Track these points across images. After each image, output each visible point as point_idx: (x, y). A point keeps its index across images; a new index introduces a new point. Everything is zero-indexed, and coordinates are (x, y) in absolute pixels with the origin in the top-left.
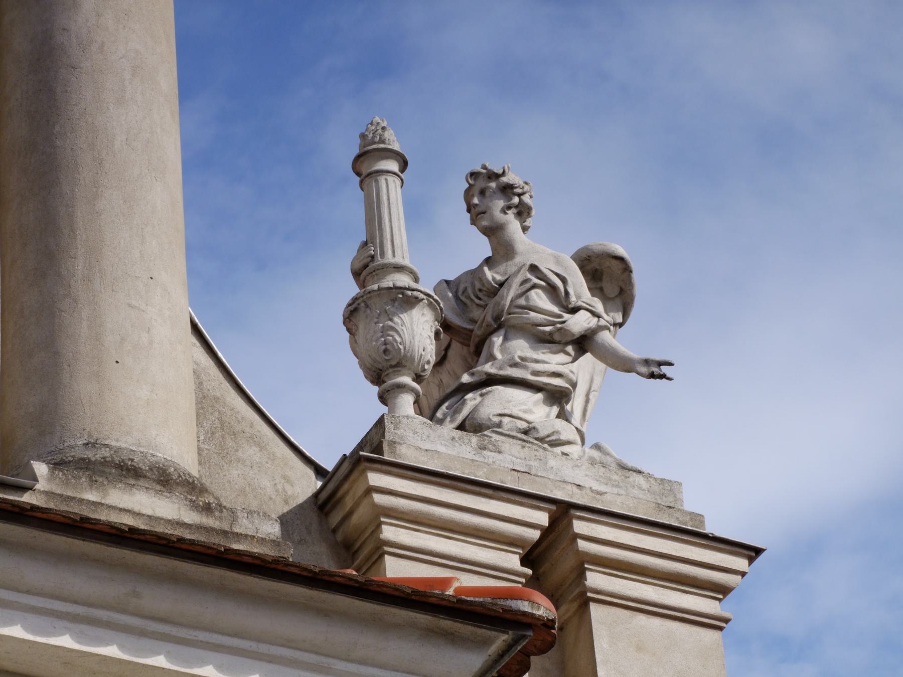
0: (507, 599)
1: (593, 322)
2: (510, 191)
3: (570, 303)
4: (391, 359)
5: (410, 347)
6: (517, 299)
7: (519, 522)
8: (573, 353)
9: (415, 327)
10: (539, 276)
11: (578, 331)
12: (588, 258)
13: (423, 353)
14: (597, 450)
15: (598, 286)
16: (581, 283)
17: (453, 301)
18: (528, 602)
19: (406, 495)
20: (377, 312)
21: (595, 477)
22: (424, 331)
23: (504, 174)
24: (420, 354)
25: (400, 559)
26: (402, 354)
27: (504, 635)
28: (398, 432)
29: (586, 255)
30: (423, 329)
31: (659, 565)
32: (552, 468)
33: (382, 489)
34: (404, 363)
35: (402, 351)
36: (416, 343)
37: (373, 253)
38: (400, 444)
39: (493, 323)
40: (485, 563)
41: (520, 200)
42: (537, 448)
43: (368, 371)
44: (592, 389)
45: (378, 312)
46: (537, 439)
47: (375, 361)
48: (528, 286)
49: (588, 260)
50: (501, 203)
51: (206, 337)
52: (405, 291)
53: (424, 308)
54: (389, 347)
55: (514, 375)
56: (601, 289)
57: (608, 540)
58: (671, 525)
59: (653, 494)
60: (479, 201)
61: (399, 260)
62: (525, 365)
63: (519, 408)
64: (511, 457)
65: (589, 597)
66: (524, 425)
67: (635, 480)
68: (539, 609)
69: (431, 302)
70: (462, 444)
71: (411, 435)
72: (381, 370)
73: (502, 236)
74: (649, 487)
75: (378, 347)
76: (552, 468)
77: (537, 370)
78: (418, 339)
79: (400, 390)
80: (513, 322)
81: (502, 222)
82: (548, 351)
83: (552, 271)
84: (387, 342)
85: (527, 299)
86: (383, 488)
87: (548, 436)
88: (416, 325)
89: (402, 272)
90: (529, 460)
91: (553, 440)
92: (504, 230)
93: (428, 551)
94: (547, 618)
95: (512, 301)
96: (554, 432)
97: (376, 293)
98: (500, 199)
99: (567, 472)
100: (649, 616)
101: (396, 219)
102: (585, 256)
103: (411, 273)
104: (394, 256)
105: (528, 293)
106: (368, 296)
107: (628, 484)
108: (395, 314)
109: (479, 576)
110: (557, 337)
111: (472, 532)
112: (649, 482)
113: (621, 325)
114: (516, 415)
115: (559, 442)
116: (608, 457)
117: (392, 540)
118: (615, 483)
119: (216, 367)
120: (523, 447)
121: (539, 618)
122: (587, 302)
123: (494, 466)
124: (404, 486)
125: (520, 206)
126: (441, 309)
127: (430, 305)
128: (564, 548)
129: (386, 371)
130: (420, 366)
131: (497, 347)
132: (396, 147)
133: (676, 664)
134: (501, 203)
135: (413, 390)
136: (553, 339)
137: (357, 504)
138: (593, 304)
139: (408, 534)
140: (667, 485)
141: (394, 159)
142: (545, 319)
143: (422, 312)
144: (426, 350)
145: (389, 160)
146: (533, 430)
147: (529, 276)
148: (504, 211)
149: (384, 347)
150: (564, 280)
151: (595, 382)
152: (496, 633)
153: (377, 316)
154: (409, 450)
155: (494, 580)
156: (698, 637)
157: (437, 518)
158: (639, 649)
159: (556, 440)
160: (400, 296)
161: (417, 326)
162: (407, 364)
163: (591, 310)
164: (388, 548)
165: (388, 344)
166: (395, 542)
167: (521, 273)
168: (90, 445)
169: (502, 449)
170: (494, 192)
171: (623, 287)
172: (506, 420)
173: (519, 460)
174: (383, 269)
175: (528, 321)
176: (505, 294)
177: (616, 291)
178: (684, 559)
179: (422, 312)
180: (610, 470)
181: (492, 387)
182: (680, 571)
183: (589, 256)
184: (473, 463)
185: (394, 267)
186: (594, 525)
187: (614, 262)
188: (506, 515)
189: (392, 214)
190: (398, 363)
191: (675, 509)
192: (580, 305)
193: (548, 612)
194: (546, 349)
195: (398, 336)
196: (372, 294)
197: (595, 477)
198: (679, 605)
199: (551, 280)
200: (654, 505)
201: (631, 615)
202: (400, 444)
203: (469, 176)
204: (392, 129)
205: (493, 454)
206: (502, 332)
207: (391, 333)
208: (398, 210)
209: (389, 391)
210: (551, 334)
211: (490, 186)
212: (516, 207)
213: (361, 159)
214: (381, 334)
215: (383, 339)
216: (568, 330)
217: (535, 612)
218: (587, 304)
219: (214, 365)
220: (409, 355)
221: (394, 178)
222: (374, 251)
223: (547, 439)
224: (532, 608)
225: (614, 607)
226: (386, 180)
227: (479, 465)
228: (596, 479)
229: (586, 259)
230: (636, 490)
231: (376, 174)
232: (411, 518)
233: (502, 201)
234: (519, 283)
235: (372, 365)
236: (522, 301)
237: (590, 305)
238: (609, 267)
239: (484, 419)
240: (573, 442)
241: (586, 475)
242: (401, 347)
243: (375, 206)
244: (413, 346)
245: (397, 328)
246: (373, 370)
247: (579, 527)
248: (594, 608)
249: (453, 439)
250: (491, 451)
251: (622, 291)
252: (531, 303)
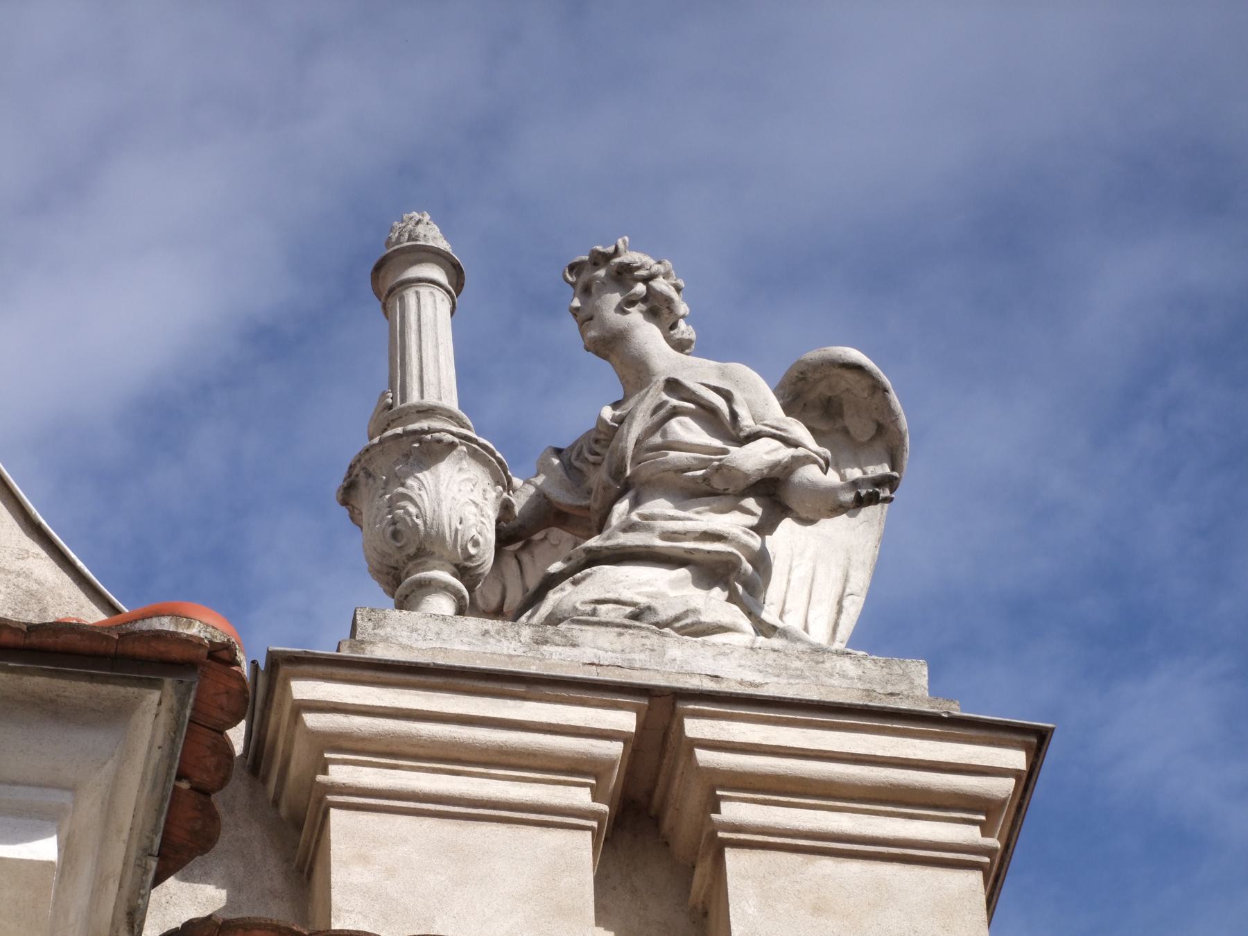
0: (136, 621)
1: (785, 453)
2: (628, 276)
3: (741, 430)
4: (406, 545)
5: (433, 519)
6: (648, 438)
7: (582, 732)
8: (759, 510)
9: (442, 489)
10: (685, 396)
11: (754, 468)
12: (801, 376)
13: (459, 527)
14: (782, 637)
15: (838, 426)
16: (766, 400)
17: (561, 472)
18: (169, 618)
19: (364, 709)
20: (382, 479)
21: (758, 667)
22: (461, 493)
23: (616, 252)
24: (453, 528)
25: (358, 812)
26: (422, 533)
27: (152, 691)
28: (381, 632)
29: (798, 372)
30: (460, 490)
31: (854, 775)
32: (675, 660)
33: (319, 704)
34: (428, 547)
35: (422, 527)
36: (445, 513)
37: (390, 401)
38: (371, 643)
39: (612, 482)
40: (516, 801)
41: (649, 288)
42: (649, 634)
43: (380, 576)
44: (848, 591)
45: (384, 478)
46: (657, 624)
47: (384, 555)
48: (662, 412)
49: (803, 379)
50: (616, 298)
51: (58, 542)
52: (424, 436)
53: (461, 459)
54: (399, 526)
55: (629, 543)
56: (846, 431)
57: (751, 744)
58: (867, 706)
59: (868, 682)
60: (581, 302)
61: (431, 399)
62: (648, 525)
63: (638, 591)
64: (595, 650)
65: (721, 838)
66: (629, 610)
67: (835, 666)
68: (190, 625)
69: (476, 450)
70: (503, 640)
71: (405, 634)
72: (395, 568)
73: (626, 351)
74: (861, 673)
75: (384, 530)
76: (675, 660)
77: (671, 530)
78: (449, 506)
79: (424, 590)
80: (645, 475)
81: (620, 327)
82: (708, 508)
83: (708, 386)
84: (396, 519)
85: (664, 435)
86: (320, 701)
87: (677, 619)
88: (445, 485)
89: (434, 417)
90: (629, 653)
91: (687, 624)
92: (627, 340)
93: (408, 792)
94: (211, 642)
95: (638, 442)
96: (687, 611)
97: (378, 449)
98: (614, 292)
99: (702, 664)
100: (840, 859)
101: (429, 346)
102: (797, 374)
103: (451, 417)
104: (422, 397)
105: (666, 425)
106: (367, 456)
107: (821, 672)
108: (408, 475)
109: (509, 825)
110: (717, 484)
111: (496, 759)
112: (862, 666)
113: (890, 482)
114: (629, 600)
115: (701, 627)
116: (798, 644)
117: (339, 781)
118: (794, 673)
119: (74, 585)
120: (621, 634)
121: (189, 641)
122: (772, 424)
123: (553, 661)
124: (359, 696)
125: (651, 298)
126: (500, 462)
127: (474, 454)
128: (683, 773)
129: (404, 568)
130: (459, 550)
131: (617, 516)
132: (443, 245)
133: (890, 928)
134: (616, 298)
135: (445, 588)
136: (712, 487)
137: (290, 742)
138: (784, 426)
139: (377, 774)
140: (896, 667)
141: (445, 270)
142: (695, 458)
143: (458, 467)
144: (464, 522)
145: (424, 264)
146: (648, 612)
147: (665, 397)
148: (621, 309)
149: (391, 528)
150: (728, 396)
151: (852, 579)
152: (136, 690)
153: (383, 485)
154: (388, 650)
155: (539, 828)
156: (936, 884)
157: (425, 740)
158: (817, 910)
159: (693, 624)
160: (416, 445)
161: (447, 486)
162: (436, 549)
163: (780, 436)
164: (336, 797)
165: (398, 522)
166: (344, 784)
167: (649, 395)
168: (144, 878)
169: (580, 640)
170: (603, 283)
171: (880, 419)
172: (600, 607)
173: (610, 653)
174: (400, 417)
175: (667, 466)
176: (625, 432)
177: (871, 430)
178: (900, 761)
179: (458, 467)
180: (786, 655)
181: (593, 568)
182: (895, 782)
183: (802, 373)
184: (511, 660)
185: (418, 412)
186: (724, 724)
187: (850, 376)
188: (554, 721)
189: (422, 339)
190: (418, 549)
191: (901, 696)
192: (759, 430)
193: (210, 629)
194: (701, 506)
195: (413, 506)
196: (372, 452)
197: (758, 667)
198: (893, 834)
199: (703, 398)
200: (860, 693)
201: (806, 861)
202: (371, 643)
203: (567, 270)
204: (435, 219)
205: (560, 649)
206: (631, 494)
207: (402, 503)
208: (436, 333)
209: (407, 596)
210: (705, 478)
211: (594, 276)
212: (644, 300)
213: (382, 274)
214: (389, 509)
215: (390, 516)
216: (733, 467)
217: (180, 630)
218: (773, 427)
219: (71, 581)
220: (433, 532)
221: (432, 290)
222: (392, 398)
223: (678, 625)
224: (177, 625)
225: (773, 852)
226: (417, 293)
227: (522, 662)
228: (758, 669)
229: (800, 380)
230: (835, 680)
231: (400, 289)
232: (381, 748)
233: (618, 294)
234: (649, 412)
235: (380, 563)
236: (657, 439)
237: (777, 429)
238: (847, 390)
239: (565, 610)
240: (732, 627)
241: (740, 666)
242: (419, 521)
243: (398, 334)
244: (439, 516)
245: (410, 493)
246: (385, 571)
247: (694, 728)
248: (730, 855)
249: (486, 633)
250: (559, 645)
251: (881, 429)
252: (671, 438)
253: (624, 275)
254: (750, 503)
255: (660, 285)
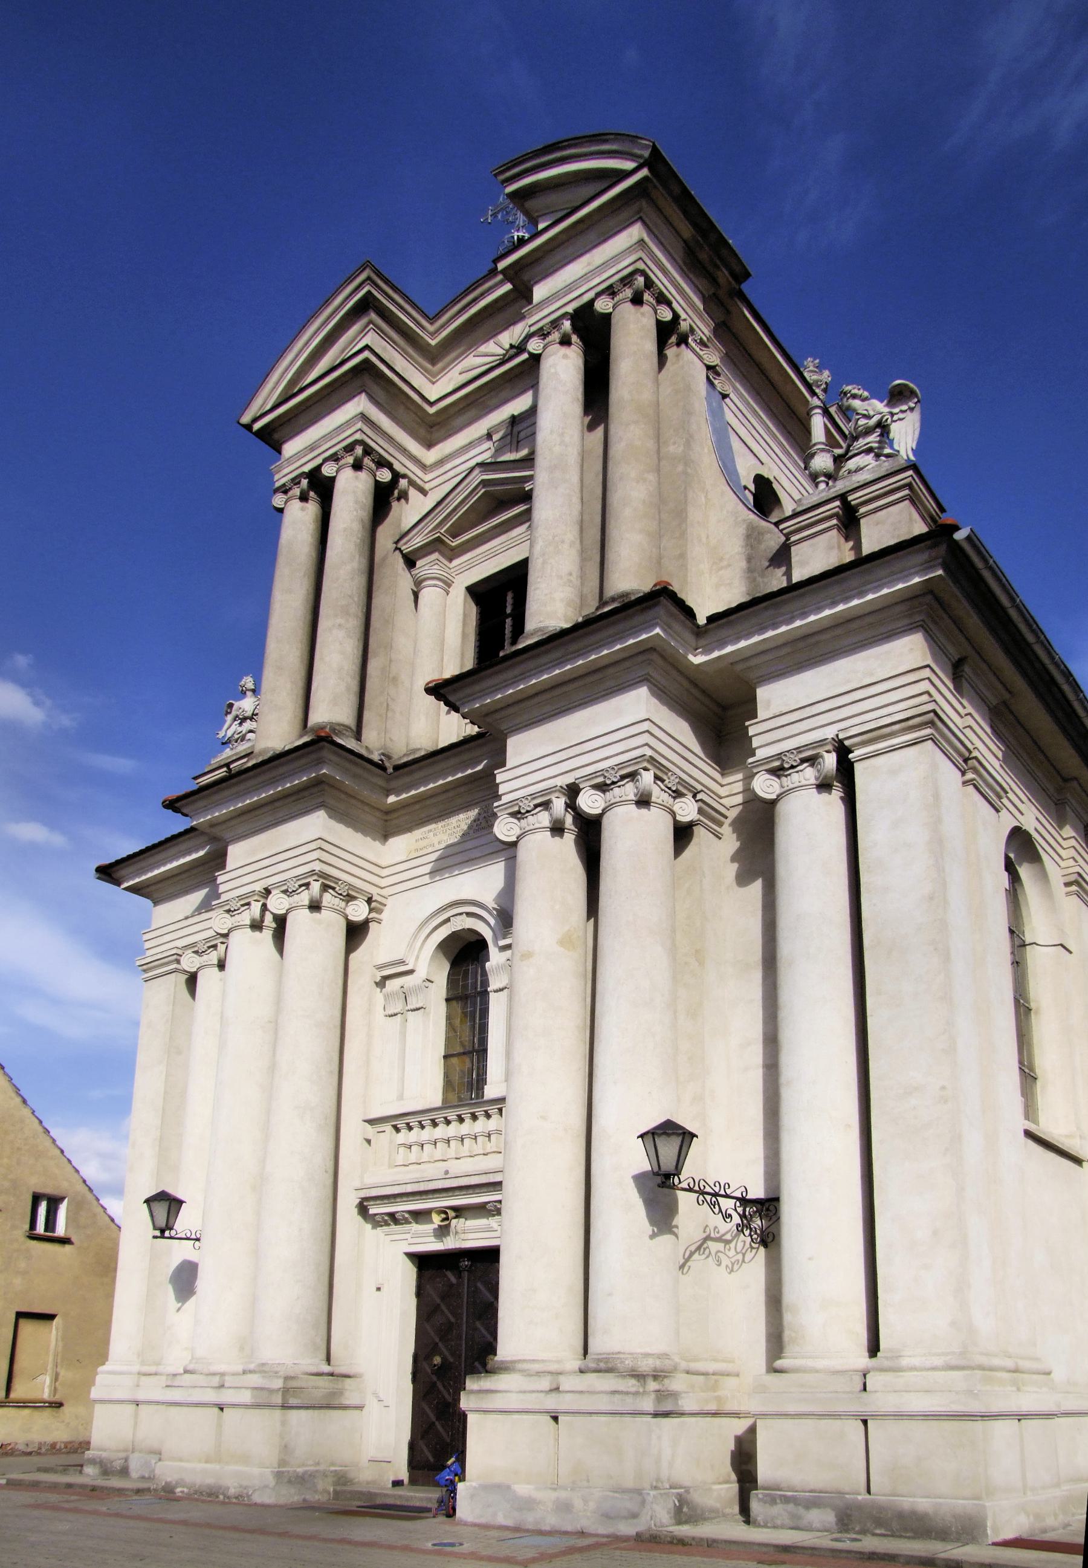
110: (868, 430)
135: (821, 481)
253: (845, 394)
254: (877, 430)
255: (853, 392)
